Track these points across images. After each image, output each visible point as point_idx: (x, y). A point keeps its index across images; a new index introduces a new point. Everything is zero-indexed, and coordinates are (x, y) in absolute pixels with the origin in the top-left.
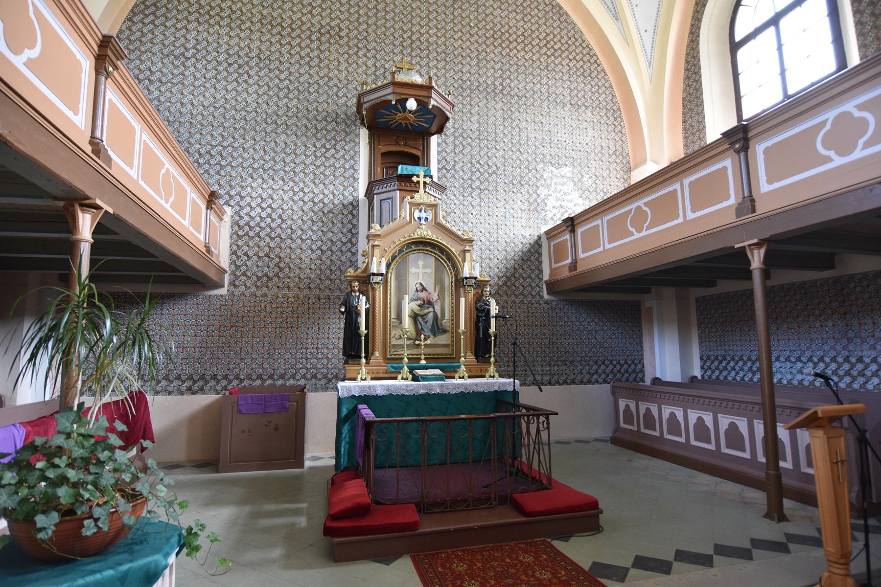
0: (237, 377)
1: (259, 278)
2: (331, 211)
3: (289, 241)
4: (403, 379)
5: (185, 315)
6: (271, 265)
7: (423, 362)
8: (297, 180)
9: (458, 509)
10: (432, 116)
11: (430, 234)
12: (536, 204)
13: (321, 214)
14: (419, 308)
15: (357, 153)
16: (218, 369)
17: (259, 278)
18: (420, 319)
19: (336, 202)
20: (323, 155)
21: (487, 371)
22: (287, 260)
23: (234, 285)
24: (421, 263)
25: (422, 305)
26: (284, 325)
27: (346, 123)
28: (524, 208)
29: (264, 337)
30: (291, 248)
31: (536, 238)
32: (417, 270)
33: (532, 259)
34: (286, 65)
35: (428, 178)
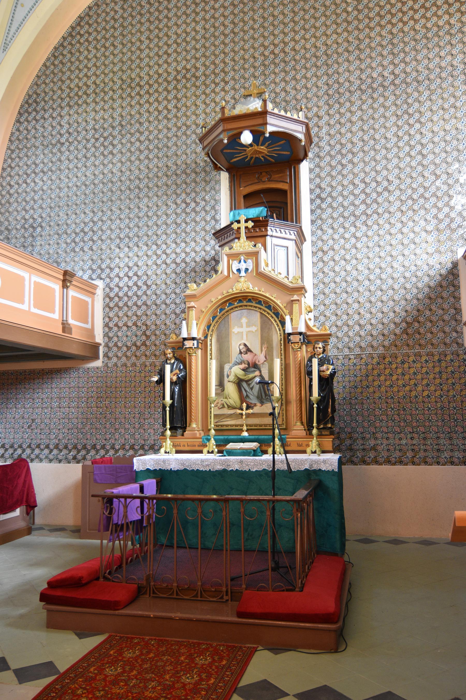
0: (113, 447)
1: (128, 348)
2: (194, 270)
3: (154, 307)
4: (209, 452)
5: (70, 388)
6: (139, 333)
7: (245, 434)
8: (159, 243)
9: (162, 595)
10: (225, 151)
11: (251, 286)
12: (448, 220)
13: (183, 274)
14: (243, 372)
15: (217, 202)
16: (97, 439)
17: (128, 348)
18: (244, 384)
19: (198, 259)
20: (184, 211)
21: (308, 445)
22: (153, 327)
23: (108, 357)
24: (244, 321)
25: (247, 368)
26: (152, 395)
27: (205, 171)
28: (429, 228)
29: (135, 407)
30: (156, 315)
31: (450, 265)
32: (240, 330)
33: (445, 294)
34: (146, 125)
35: (250, 222)
